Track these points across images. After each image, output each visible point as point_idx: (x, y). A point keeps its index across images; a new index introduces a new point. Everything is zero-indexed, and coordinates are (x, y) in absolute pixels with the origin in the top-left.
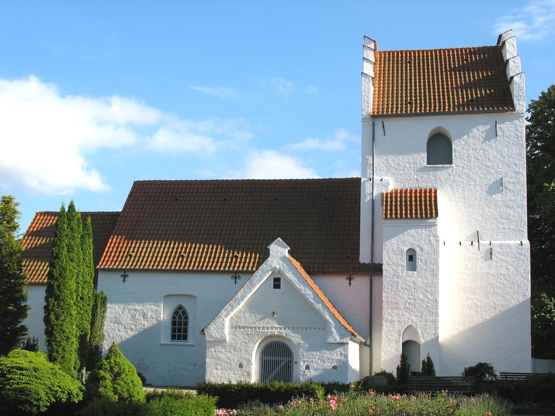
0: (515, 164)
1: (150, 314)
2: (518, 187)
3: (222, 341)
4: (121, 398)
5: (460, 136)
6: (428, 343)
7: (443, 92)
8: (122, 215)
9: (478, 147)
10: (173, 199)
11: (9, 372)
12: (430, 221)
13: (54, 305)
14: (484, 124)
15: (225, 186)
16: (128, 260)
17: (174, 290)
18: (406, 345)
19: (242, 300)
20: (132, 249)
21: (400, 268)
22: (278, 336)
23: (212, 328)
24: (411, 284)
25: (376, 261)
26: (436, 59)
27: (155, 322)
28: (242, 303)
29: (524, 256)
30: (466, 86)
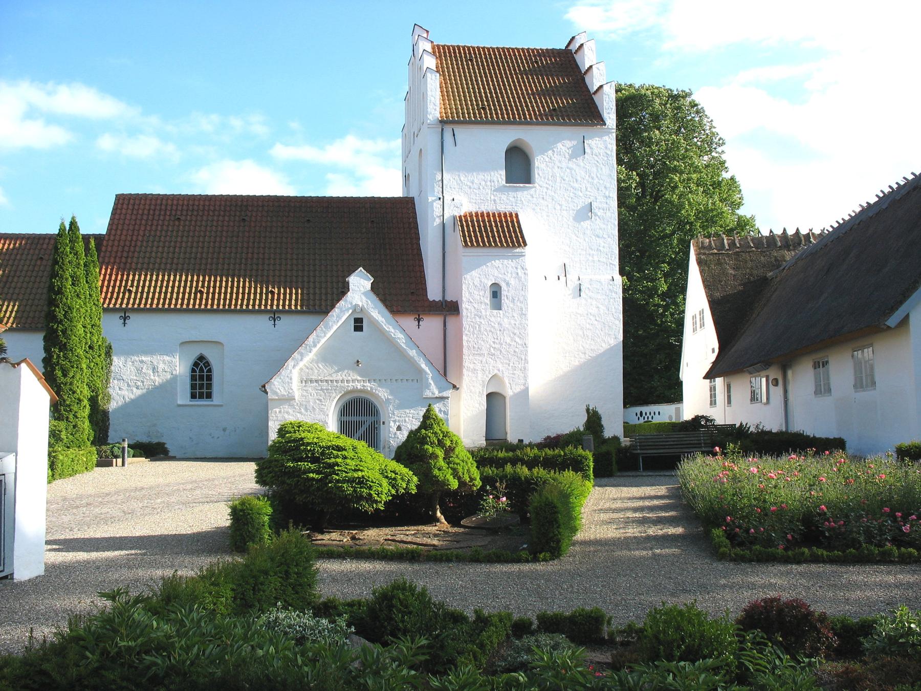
0: (605, 187)
1: (161, 366)
2: (608, 214)
3: (289, 400)
4: (462, 483)
5: (543, 151)
6: (517, 396)
7: (519, 98)
8: (106, 238)
9: (564, 165)
10: (172, 218)
11: (323, 454)
12: (518, 250)
13: (58, 356)
14: (570, 140)
15: (240, 203)
16: (127, 296)
17: (195, 336)
18: (491, 397)
19: (315, 346)
20: (130, 283)
21: (483, 306)
22: (361, 391)
23: (276, 383)
24: (496, 326)
25: (449, 298)
26: (501, 58)
27: (169, 376)
28: (315, 350)
29: (616, 293)
30: (545, 93)
